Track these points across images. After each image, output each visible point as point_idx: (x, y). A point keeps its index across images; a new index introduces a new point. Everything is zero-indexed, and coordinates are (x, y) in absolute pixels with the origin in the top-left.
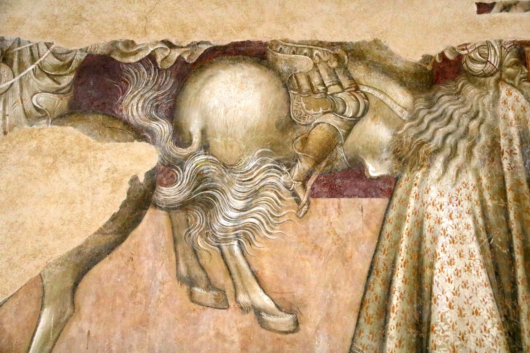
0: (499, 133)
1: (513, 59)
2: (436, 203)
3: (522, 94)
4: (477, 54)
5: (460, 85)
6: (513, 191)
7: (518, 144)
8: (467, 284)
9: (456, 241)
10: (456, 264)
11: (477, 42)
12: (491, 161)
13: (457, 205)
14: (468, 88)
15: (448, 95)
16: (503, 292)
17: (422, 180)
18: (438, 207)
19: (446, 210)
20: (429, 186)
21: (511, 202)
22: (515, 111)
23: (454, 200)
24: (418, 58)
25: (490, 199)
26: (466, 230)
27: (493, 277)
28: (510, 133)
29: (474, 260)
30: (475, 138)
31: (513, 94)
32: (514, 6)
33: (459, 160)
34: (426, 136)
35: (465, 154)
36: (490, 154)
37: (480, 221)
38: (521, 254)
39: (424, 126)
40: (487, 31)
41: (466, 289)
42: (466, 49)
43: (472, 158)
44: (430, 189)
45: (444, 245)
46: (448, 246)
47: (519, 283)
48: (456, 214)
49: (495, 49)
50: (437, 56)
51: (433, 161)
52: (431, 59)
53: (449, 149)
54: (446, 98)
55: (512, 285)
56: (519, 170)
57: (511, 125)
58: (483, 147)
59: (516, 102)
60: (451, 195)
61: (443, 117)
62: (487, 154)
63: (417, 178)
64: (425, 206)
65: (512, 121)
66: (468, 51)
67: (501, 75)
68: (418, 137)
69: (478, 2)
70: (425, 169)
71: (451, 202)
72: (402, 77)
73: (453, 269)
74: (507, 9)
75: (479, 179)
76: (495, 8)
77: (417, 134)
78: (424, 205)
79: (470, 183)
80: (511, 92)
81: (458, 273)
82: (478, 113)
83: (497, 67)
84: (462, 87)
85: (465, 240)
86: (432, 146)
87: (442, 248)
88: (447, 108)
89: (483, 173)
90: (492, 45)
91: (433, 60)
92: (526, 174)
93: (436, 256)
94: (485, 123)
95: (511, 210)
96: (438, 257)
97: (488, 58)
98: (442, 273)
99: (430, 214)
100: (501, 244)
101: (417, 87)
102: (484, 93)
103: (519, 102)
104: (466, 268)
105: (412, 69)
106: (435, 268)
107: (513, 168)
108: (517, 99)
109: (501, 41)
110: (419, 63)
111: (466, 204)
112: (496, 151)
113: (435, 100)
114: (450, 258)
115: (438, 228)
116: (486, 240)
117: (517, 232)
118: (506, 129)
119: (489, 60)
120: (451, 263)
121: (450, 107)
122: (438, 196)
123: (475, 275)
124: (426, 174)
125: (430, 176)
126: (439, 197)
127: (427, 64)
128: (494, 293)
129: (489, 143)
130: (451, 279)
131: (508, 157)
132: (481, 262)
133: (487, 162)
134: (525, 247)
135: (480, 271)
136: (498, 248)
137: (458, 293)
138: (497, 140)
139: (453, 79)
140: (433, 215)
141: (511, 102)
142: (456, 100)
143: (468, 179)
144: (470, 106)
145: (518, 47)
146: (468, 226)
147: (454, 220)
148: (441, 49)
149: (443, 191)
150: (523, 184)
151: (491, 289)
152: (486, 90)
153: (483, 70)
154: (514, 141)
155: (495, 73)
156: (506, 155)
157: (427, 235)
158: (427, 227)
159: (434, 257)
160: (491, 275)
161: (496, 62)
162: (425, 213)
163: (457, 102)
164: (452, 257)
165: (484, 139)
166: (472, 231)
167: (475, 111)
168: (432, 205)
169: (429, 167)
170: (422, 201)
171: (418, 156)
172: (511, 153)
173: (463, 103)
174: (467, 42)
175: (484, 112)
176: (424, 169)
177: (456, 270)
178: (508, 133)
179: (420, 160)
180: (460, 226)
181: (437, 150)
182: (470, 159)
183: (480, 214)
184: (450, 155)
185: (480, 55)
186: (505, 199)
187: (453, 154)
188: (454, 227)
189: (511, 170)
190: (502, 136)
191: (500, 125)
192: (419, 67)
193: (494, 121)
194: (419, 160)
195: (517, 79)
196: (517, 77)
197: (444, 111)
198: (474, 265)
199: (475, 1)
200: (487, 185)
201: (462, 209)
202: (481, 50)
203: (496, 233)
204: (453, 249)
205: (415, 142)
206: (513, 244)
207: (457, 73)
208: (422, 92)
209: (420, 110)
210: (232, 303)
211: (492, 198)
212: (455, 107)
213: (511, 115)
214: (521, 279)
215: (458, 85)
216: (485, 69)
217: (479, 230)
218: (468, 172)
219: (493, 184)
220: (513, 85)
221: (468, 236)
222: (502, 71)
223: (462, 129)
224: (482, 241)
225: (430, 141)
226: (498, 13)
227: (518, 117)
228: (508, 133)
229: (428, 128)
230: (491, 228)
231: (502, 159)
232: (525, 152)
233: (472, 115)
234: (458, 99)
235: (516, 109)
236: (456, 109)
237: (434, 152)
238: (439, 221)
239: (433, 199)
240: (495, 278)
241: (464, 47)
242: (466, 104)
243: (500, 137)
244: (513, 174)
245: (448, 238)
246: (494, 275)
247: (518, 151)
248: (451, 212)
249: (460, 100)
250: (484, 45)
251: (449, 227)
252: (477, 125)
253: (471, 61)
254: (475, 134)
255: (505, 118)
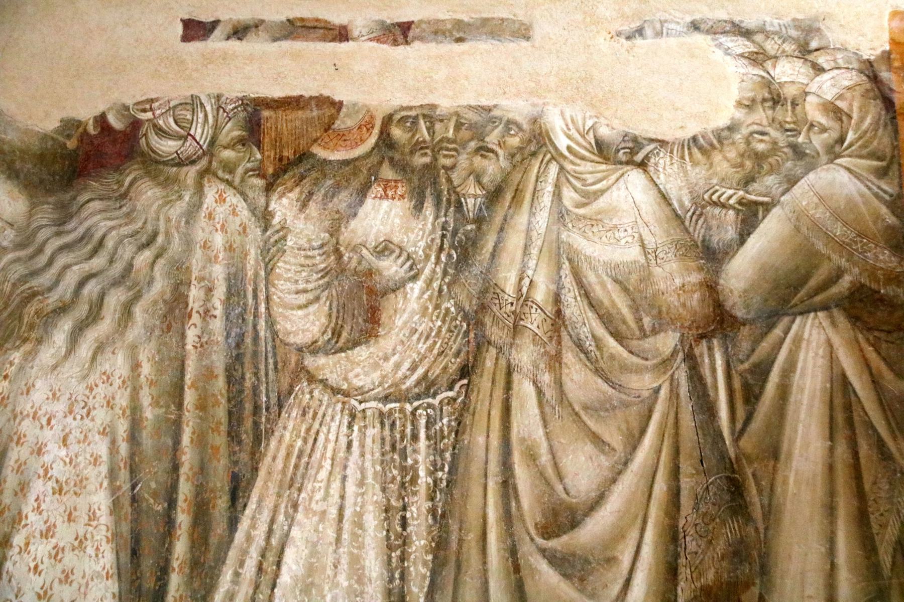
0: (191, 275)
1: (236, 133)
2: (40, 413)
3: (245, 200)
4: (171, 120)
5: (128, 180)
6: (197, 389)
7: (223, 298)
8: (70, 575)
9: (65, 488)
10: (57, 535)
11: (174, 95)
12: (165, 330)
13: (82, 418)
14: (143, 186)
15: (101, 199)
16: (139, 588)
17: (21, 368)
18: (44, 422)
19: (58, 428)
20: (33, 378)
21: (188, 411)
22: (226, 233)
23: (77, 409)
24: (50, 125)
25: (150, 404)
26: (91, 467)
27: (125, 557)
28: (210, 276)
29: (96, 527)
30: (141, 284)
31: (228, 199)
32: (254, 29)
33: (105, 326)
34: (37, 283)
35: (117, 316)
36: (165, 316)
37: (124, 448)
38: (189, 514)
39: (43, 259)
40: (195, 75)
41: (68, 585)
42: (151, 109)
43: (130, 324)
44: (34, 386)
45: (41, 497)
46: (47, 499)
47: (174, 569)
48: (78, 435)
49: (205, 111)
50: (91, 122)
51: (49, 329)
52: (78, 127)
53: (87, 307)
54: (96, 205)
55: (159, 574)
56: (215, 348)
57: (216, 262)
58: (155, 302)
59: (231, 217)
60: (73, 399)
61: (84, 242)
62: (159, 317)
63: (11, 364)
64: (18, 420)
65: (218, 252)
66: (153, 114)
67: (210, 162)
68: (26, 282)
69: (186, 17)
70: (31, 345)
71: (71, 412)
72: (13, 162)
73: (49, 547)
74: (240, 35)
75: (136, 366)
76: (217, 32)
77: (26, 276)
78: (15, 418)
79: (117, 374)
80: (225, 196)
81: (57, 554)
82: (155, 235)
83: (204, 147)
84: (132, 184)
85: (85, 487)
86: (50, 301)
87: (36, 505)
88: (95, 225)
89: (144, 356)
90: (202, 104)
91: (81, 130)
92: (226, 356)
93: (20, 520)
94: (166, 256)
95: (188, 426)
96: (23, 523)
97: (190, 129)
98: (25, 555)
99: (25, 436)
100: (155, 495)
101: (42, 181)
102: (174, 197)
103: (237, 215)
104: (76, 543)
105: (35, 145)
106: (11, 546)
107: (203, 346)
108: (234, 209)
109: (218, 97)
110: (52, 134)
111: (101, 416)
112: (177, 311)
113: (75, 208)
114: (48, 524)
115: (35, 465)
116: (127, 487)
117: (191, 469)
118: (204, 267)
119: (192, 132)
120: (48, 533)
121: (102, 224)
122: (48, 399)
123: (90, 557)
124: (30, 356)
125: (37, 360)
126: (50, 401)
127: (69, 137)
128: (120, 592)
129: (168, 296)
130: (41, 567)
131: (199, 325)
132: (108, 531)
133: (157, 332)
134: (198, 499)
135: (102, 549)
136: (147, 500)
137: (49, 593)
138: (183, 289)
139: (117, 169)
140: (31, 439)
141: (221, 216)
142: (115, 209)
143: (114, 365)
144: (143, 221)
145: (249, 109)
146: (96, 460)
147: (71, 447)
148: (101, 108)
149: (59, 390)
150: (216, 376)
151: (117, 585)
152: (178, 192)
153: (176, 152)
154: (215, 292)
155: (199, 158)
156: (195, 318)
157: (9, 479)
158: (12, 463)
159: (14, 522)
160: (122, 555)
161: (204, 136)
162: (15, 434)
163: (117, 213)
164: (53, 521)
165: (160, 286)
166: (104, 469)
167: (150, 232)
168: (31, 419)
169: (40, 341)
170: (14, 410)
171: (20, 318)
172: (207, 314)
173: (128, 215)
174: (153, 96)
175: (167, 233)
176: (28, 347)
177: (54, 548)
178: (208, 275)
179: (24, 327)
180: (80, 458)
181: (60, 308)
182: (126, 327)
183: (125, 435)
184: (87, 318)
185: (176, 122)
186: (180, 405)
187: (94, 315)
188: (68, 460)
189: (199, 349)
190: (194, 282)
191: (194, 260)
192: (50, 143)
193: (184, 251)
194: (20, 328)
195: (240, 171)
196: (241, 167)
197: (88, 230)
198: (93, 537)
199: (181, 16)
200: (150, 378)
201: (91, 425)
202: (178, 112)
203: (150, 472)
204: (56, 505)
205: (19, 291)
206: (177, 493)
207: (126, 157)
208: (49, 192)
209: (40, 227)
210: (737, 206)
211: (155, 403)
212: (110, 223)
213: (219, 240)
214: (179, 562)
215: (123, 181)
216: (182, 149)
217: (117, 468)
218: (116, 351)
219: (161, 375)
220: (229, 183)
221: (92, 479)
222: (212, 155)
223: (118, 268)
224: (120, 488)
225: (50, 289)
226: (220, 41)
227: (231, 246)
228: (208, 275)
229: (50, 263)
230: (141, 461)
231: (187, 327)
232: (232, 314)
233: (144, 239)
234: (121, 207)
235: (229, 230)
236: (113, 228)
237: (54, 311)
238: (39, 451)
239: (37, 405)
240: (129, 561)
241: (148, 106)
242: (134, 218)
243: (189, 284)
244: (201, 356)
245: (51, 484)
246: (129, 555)
247: (219, 311)
248: (67, 430)
249: (124, 209)
250: (186, 104)
251: (58, 460)
252: (150, 260)
253: (156, 134)
254: (142, 277)
255: (205, 246)
